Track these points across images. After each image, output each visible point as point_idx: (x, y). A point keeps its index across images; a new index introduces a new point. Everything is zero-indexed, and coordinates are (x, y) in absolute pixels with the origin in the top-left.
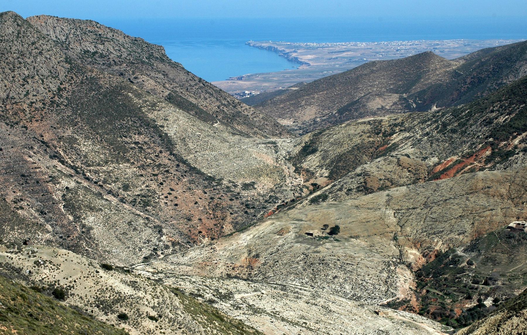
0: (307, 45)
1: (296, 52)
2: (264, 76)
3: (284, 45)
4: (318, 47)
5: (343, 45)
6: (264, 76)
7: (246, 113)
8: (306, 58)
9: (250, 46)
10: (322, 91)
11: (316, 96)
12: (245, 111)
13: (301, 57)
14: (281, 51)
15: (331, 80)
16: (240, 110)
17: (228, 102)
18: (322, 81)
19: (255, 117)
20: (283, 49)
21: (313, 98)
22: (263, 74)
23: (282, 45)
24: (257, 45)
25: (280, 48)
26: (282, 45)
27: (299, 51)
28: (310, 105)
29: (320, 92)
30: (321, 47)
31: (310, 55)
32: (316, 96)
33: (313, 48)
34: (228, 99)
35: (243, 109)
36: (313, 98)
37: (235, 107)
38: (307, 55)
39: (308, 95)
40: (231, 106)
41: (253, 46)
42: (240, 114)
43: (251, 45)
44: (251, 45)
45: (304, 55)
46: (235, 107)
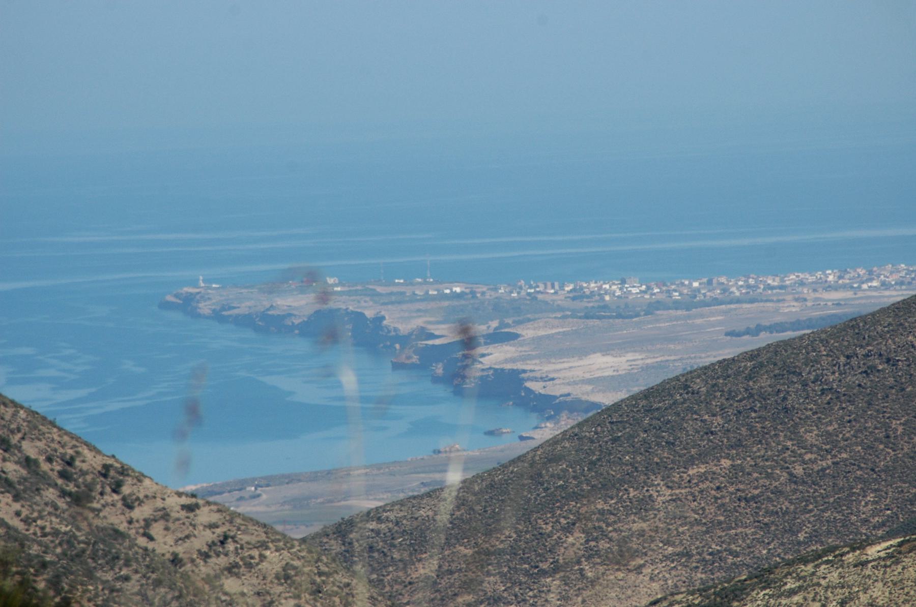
0: (578, 295)
1: (511, 337)
2: (294, 490)
3: (427, 298)
4: (656, 306)
5: (829, 288)
6: (294, 490)
7: (164, 543)
8: (579, 374)
9: (196, 315)
10: (702, 457)
11: (662, 494)
12: (157, 530)
13: (547, 368)
14: (404, 340)
15: (764, 382)
16: (115, 518)
17: (28, 463)
18: (698, 385)
19: (231, 570)
20: (418, 322)
21: (643, 506)
22: (290, 479)
23: (414, 299)
24: (243, 309)
25: (400, 321)
26: (414, 299)
27: (528, 332)
28: (622, 557)
29: (692, 461)
30: (677, 305)
31: (606, 350)
32: (662, 494)
33: (624, 311)
34: (30, 449)
35: (140, 513)
36: (643, 506)
37: (79, 500)
38: (583, 352)
39: (606, 487)
40: (50, 494)
41: (218, 316)
42: (121, 547)
43: (205, 308)
44: (205, 308)
45: (563, 353)
46: (79, 500)
